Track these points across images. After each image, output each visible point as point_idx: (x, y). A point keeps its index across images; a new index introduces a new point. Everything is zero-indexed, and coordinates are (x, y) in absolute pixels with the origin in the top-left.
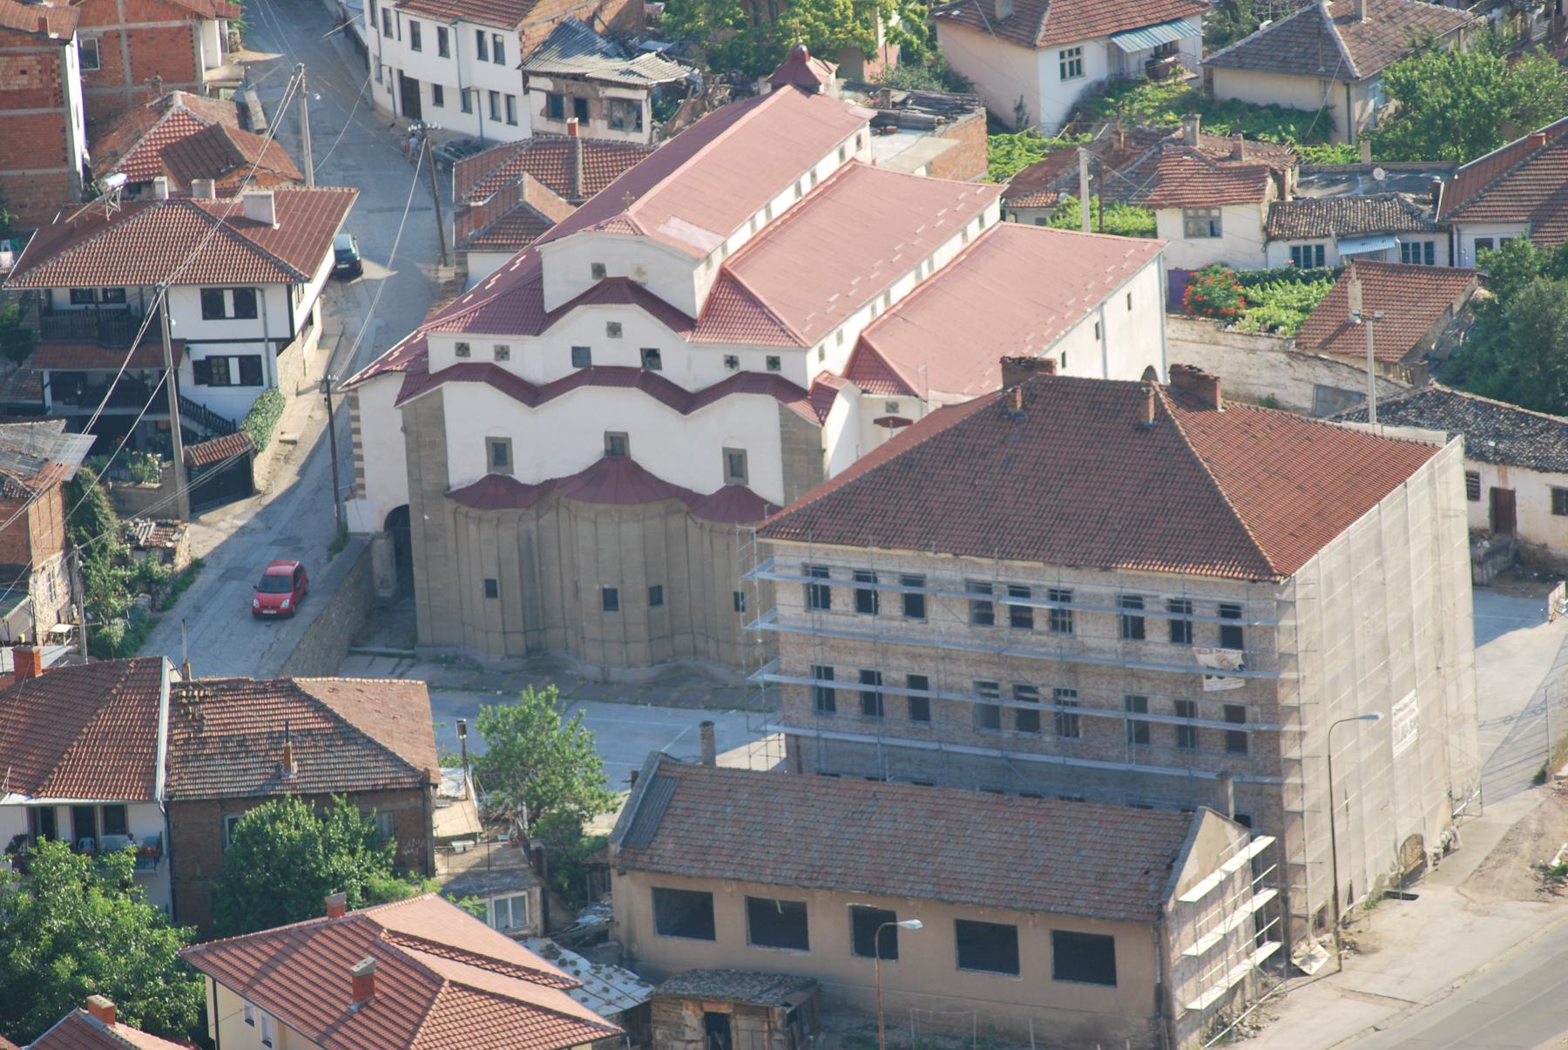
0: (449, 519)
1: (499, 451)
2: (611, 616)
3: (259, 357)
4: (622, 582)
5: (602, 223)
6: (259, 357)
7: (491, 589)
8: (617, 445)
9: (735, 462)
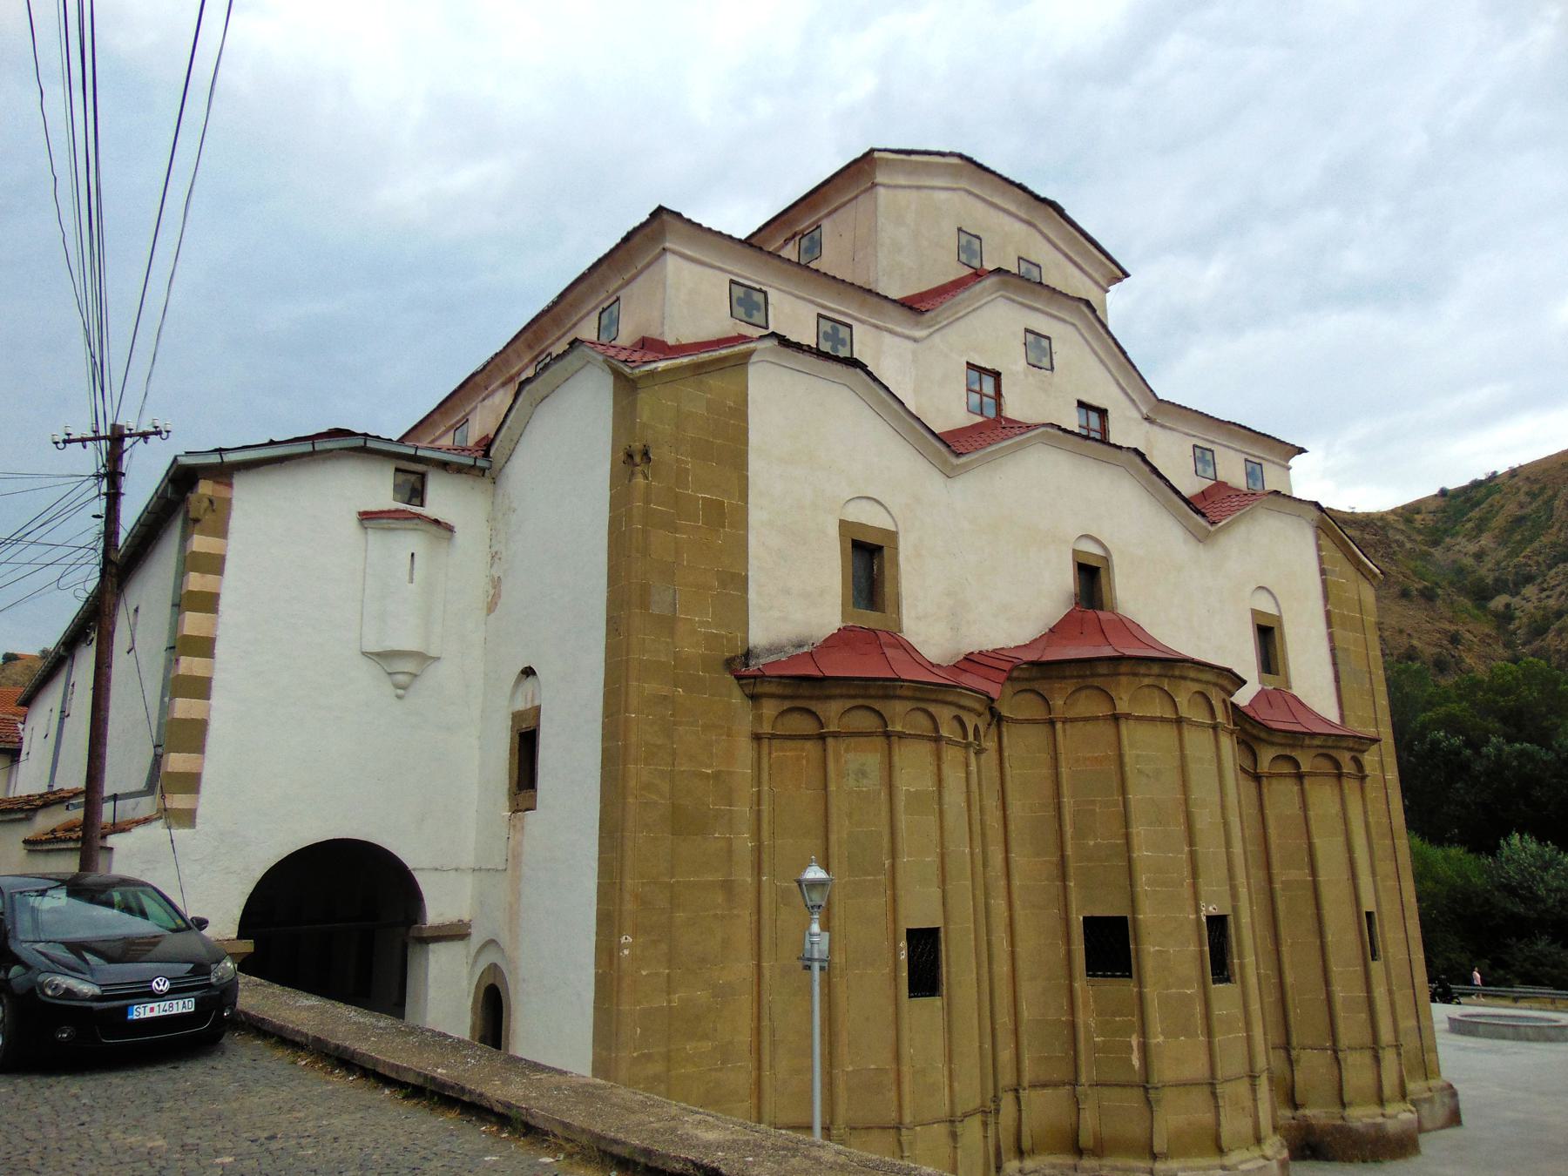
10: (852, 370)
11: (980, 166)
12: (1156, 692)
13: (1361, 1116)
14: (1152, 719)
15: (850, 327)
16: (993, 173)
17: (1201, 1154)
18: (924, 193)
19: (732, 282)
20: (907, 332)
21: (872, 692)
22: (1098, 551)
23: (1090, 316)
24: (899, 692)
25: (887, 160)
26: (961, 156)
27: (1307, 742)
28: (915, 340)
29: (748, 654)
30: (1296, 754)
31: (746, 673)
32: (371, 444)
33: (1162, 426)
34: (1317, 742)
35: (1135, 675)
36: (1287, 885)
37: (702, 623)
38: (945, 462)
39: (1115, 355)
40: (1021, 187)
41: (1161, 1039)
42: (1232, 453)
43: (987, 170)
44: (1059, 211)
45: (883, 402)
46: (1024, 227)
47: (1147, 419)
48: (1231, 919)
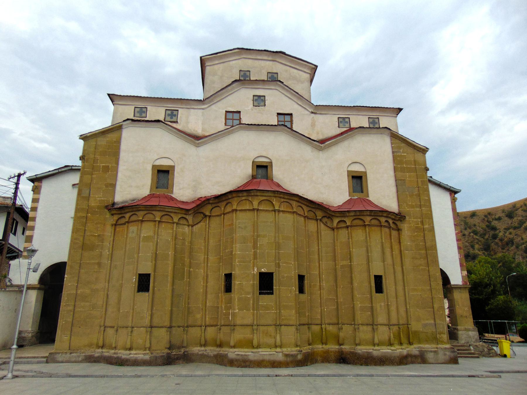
0: (109, 230)
1: (163, 174)
2: (266, 300)
3: (376, 292)
4: (278, 266)
5: (35, 177)
6: (376, 292)
7: (144, 283)
8: (262, 169)
9: (358, 180)
10: (159, 123)
11: (247, 49)
12: (248, 202)
13: (362, 349)
14: (245, 210)
15: (349, 118)
16: (253, 50)
17: (248, 348)
18: (226, 64)
19: (369, 118)
20: (199, 107)
21: (134, 210)
22: (269, 161)
23: (282, 85)
24: (140, 209)
25: (208, 58)
26: (238, 49)
27: (347, 214)
28: (203, 109)
29: (114, 204)
30: (187, 217)
31: (114, 209)
32: (73, 168)
33: (321, 114)
34: (352, 214)
35: (239, 197)
36: (342, 267)
37: (98, 197)
38: (195, 143)
39: (295, 95)
40: (265, 50)
41: (237, 310)
42: (361, 117)
43: (250, 50)
44: (284, 53)
45: (171, 130)
46: (271, 63)
47: (312, 113)
48: (383, 277)
